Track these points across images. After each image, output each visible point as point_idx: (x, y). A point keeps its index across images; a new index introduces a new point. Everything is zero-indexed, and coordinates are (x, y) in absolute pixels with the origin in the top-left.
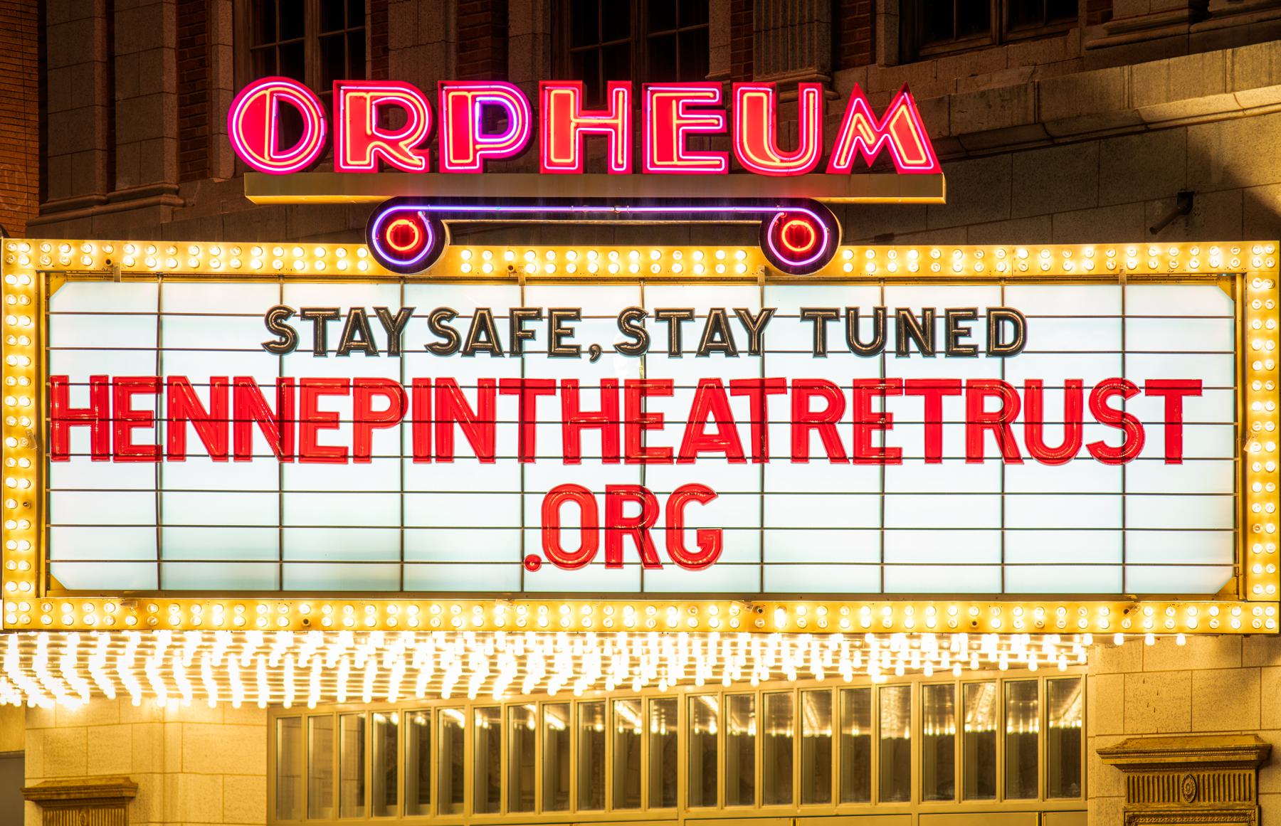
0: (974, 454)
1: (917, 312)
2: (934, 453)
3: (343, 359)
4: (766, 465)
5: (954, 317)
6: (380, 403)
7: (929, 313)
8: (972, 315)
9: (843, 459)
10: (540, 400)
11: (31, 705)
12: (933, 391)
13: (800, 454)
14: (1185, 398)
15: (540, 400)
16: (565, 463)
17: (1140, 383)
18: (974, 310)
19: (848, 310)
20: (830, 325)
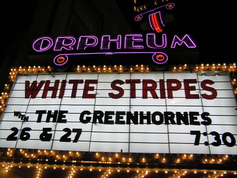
0: (145, 96)
1: (182, 113)
2: (74, 96)
3: (75, 143)
4: (185, 98)
5: (108, 113)
6: (174, 85)
7: (186, 113)
8: (112, 113)
9: (157, 98)
10: (136, 85)
11: (63, 98)
12: (75, 83)
13: (145, 96)
14: (173, 91)
15: (136, 85)
16: (186, 99)
17: (124, 81)
18: (198, 113)
19: (140, 112)
20: (43, 115)
